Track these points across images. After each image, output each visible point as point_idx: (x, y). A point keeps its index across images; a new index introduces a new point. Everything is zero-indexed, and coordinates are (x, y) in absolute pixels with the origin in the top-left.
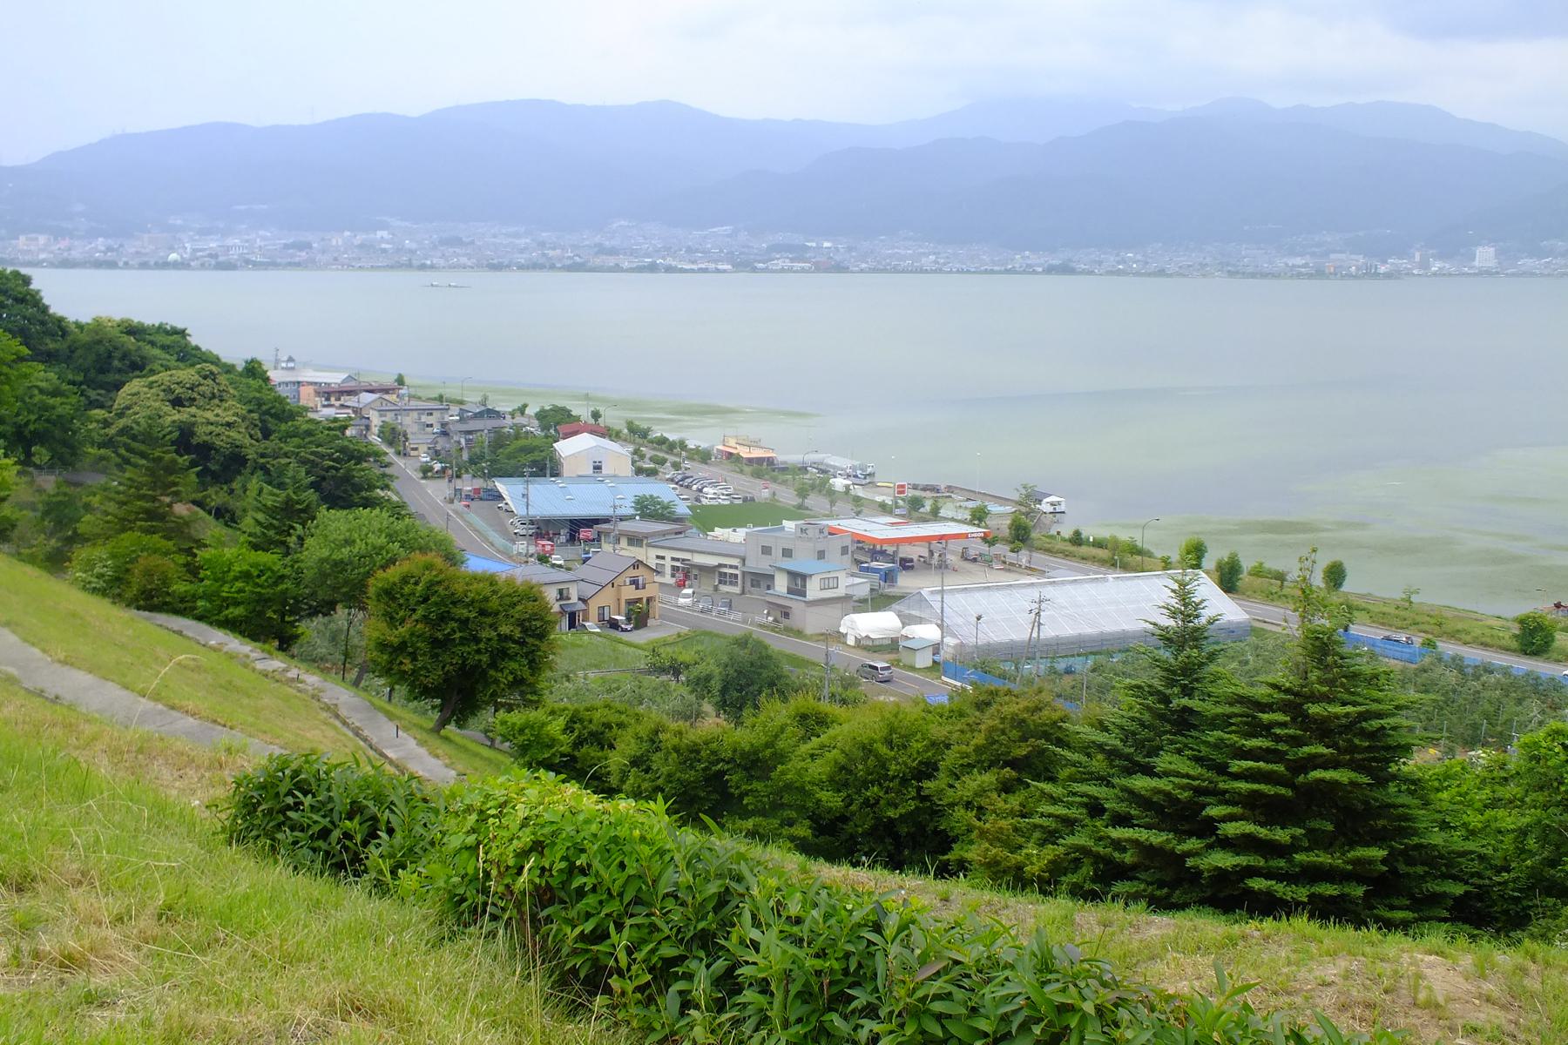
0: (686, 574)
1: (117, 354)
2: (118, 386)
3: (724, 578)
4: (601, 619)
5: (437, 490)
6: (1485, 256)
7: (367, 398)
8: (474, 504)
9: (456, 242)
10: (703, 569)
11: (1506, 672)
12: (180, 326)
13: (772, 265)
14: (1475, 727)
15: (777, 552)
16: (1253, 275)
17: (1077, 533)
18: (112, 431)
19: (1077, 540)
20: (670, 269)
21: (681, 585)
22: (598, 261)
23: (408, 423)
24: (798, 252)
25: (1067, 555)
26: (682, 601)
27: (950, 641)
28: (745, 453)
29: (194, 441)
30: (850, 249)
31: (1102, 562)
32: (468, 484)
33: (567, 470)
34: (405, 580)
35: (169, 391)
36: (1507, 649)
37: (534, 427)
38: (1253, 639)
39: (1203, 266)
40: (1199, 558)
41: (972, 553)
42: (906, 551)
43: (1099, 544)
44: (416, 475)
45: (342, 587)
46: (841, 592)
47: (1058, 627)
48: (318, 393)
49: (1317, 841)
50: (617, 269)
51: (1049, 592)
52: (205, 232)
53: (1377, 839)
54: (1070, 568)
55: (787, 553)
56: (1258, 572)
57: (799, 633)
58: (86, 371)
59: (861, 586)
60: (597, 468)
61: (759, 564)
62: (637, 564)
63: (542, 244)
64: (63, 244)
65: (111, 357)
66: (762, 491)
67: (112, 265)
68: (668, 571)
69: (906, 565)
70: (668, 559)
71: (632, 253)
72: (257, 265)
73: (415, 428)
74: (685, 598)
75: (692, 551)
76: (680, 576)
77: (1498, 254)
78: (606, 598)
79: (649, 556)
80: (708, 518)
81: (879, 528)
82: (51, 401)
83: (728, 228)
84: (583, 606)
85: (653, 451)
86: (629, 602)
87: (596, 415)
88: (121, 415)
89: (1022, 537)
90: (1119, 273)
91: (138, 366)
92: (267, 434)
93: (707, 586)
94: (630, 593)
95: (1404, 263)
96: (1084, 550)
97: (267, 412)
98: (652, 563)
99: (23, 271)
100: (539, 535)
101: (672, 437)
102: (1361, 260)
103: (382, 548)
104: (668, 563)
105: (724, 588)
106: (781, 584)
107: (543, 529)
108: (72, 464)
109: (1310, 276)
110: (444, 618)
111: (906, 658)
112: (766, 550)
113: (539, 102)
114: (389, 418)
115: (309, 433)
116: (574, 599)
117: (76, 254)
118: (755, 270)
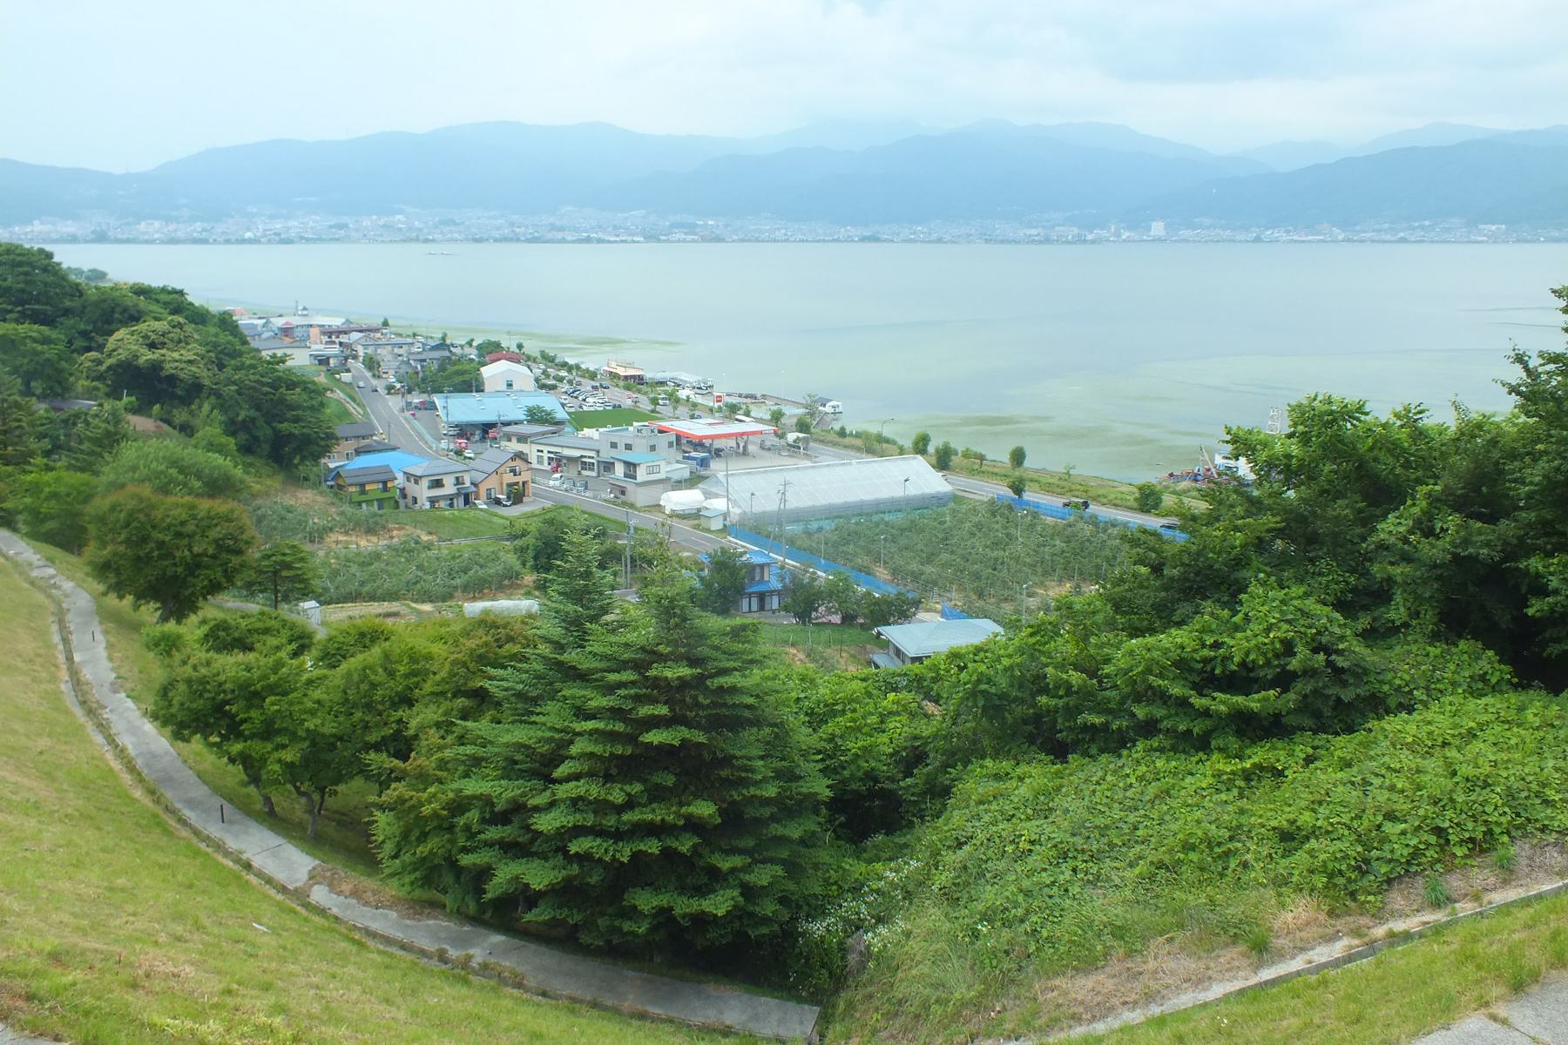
0: (558, 462)
1: (118, 309)
2: (111, 333)
3: (585, 466)
4: (489, 497)
5: (395, 403)
6: (1158, 228)
7: (355, 336)
8: (419, 414)
9: (453, 222)
10: (571, 459)
11: (1125, 525)
12: (178, 287)
13: (670, 237)
14: (1098, 567)
15: (621, 446)
16: (1002, 242)
17: (843, 429)
18: (103, 368)
19: (842, 433)
20: (600, 241)
21: (555, 470)
22: (550, 236)
23: (383, 353)
24: (690, 228)
25: (835, 444)
26: (551, 483)
27: (737, 511)
28: (622, 372)
29: (163, 374)
30: (726, 226)
31: (859, 449)
32: (416, 399)
33: (487, 388)
34: (113, 508)
35: (146, 337)
36: (1130, 508)
37: (473, 354)
38: (952, 505)
39: (969, 235)
40: (926, 445)
41: (768, 444)
42: (718, 444)
43: (858, 435)
44: (382, 391)
46: (662, 476)
47: (796, 501)
48: (324, 333)
49: (657, 795)
50: (563, 241)
51: (789, 476)
52: (272, 217)
53: (704, 790)
54: (836, 456)
55: (628, 447)
56: (966, 455)
57: (632, 506)
58: (94, 322)
59: (682, 470)
60: (510, 385)
61: (607, 454)
63: (512, 224)
64: (171, 227)
65: (116, 309)
66: (625, 399)
67: (205, 241)
69: (718, 453)
71: (576, 229)
72: (308, 240)
73: (390, 357)
74: (555, 481)
76: (554, 464)
77: (1167, 227)
78: (492, 483)
79: (531, 450)
80: (582, 420)
81: (698, 428)
82: (40, 348)
83: (643, 212)
85: (553, 371)
86: (509, 485)
87: (520, 346)
88: (109, 356)
89: (809, 431)
90: (910, 241)
91: (134, 317)
92: (221, 367)
93: (572, 471)
94: (509, 478)
95: (1104, 233)
96: (847, 441)
97: (222, 352)
99: (48, 248)
100: (460, 436)
101: (571, 361)
102: (1076, 231)
103: (162, 472)
104: (546, 455)
105: (585, 473)
106: (620, 470)
107: (463, 430)
108: (62, 395)
109: (1040, 242)
110: (145, 540)
111: (703, 521)
112: (614, 445)
114: (370, 351)
115: (253, 367)
116: (468, 484)
117: (180, 234)
118: (659, 241)
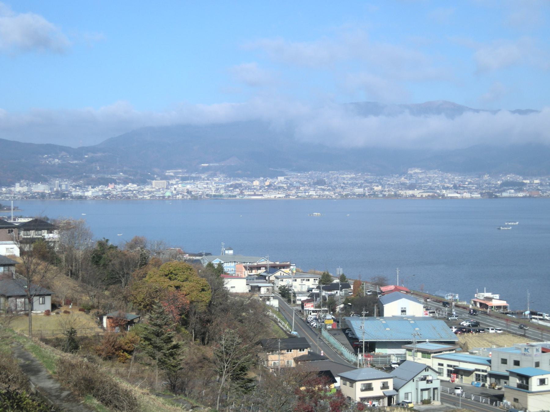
45: (209, 310)
55: (517, 363)
62: (427, 368)
68: (445, 372)
70: (445, 365)
75: (459, 361)
79: (433, 362)
84: (395, 393)
98: (436, 367)
104: (445, 369)
112: (504, 361)
113: (18, 143)
